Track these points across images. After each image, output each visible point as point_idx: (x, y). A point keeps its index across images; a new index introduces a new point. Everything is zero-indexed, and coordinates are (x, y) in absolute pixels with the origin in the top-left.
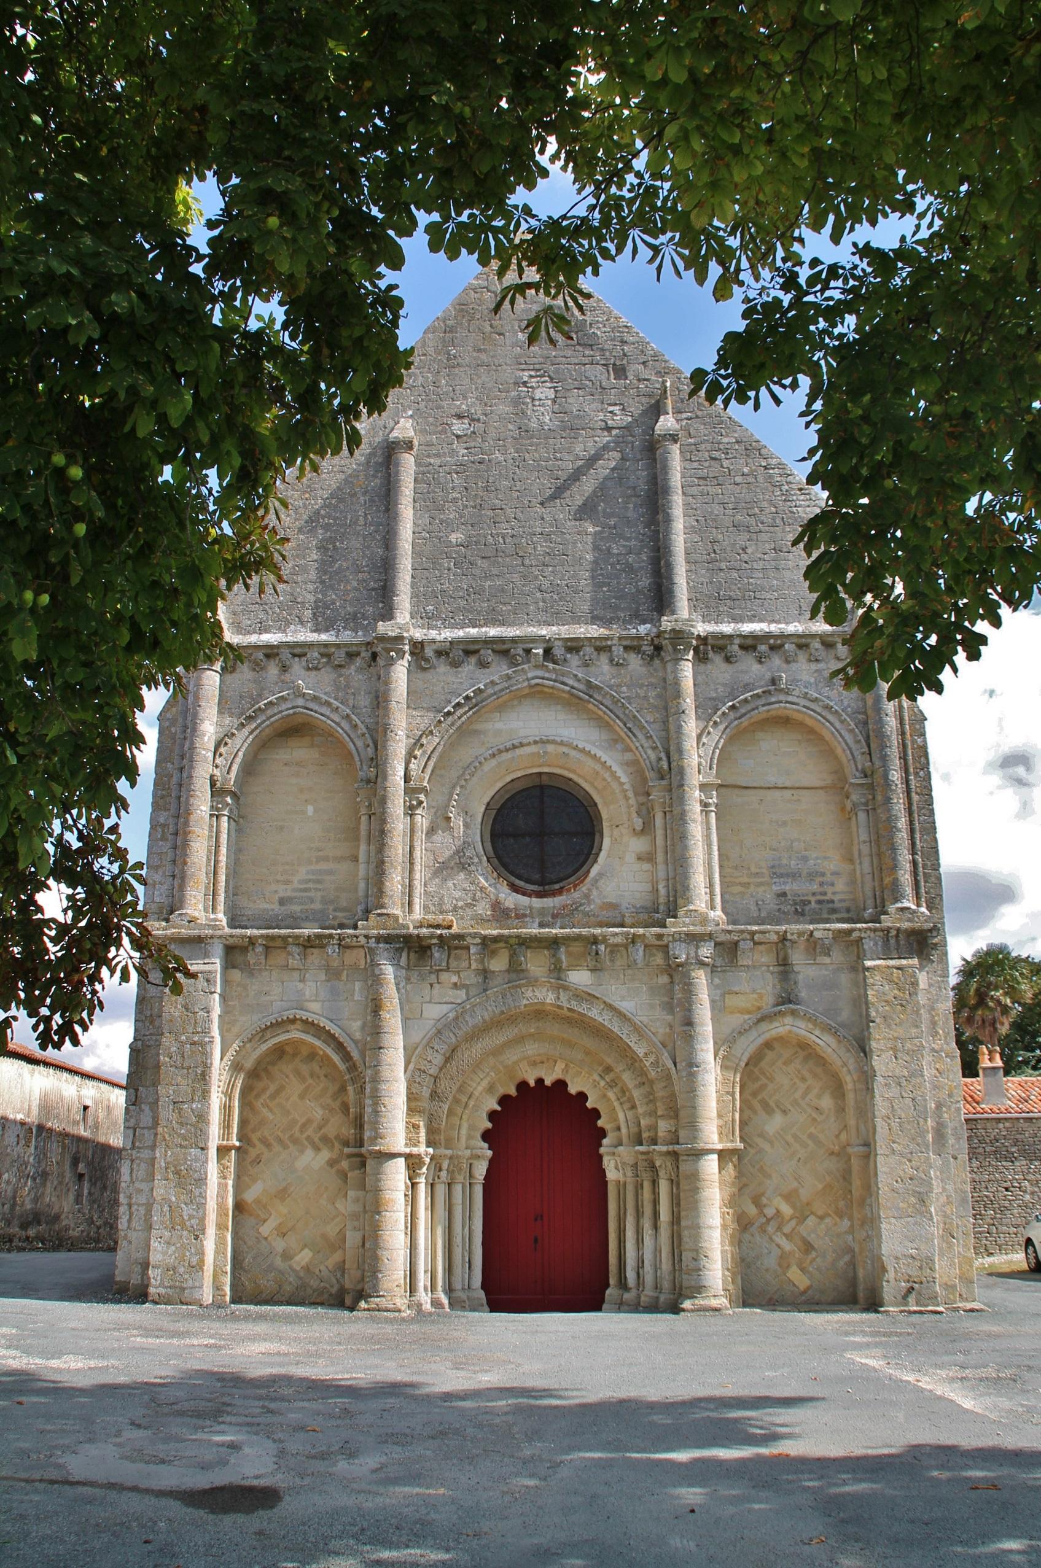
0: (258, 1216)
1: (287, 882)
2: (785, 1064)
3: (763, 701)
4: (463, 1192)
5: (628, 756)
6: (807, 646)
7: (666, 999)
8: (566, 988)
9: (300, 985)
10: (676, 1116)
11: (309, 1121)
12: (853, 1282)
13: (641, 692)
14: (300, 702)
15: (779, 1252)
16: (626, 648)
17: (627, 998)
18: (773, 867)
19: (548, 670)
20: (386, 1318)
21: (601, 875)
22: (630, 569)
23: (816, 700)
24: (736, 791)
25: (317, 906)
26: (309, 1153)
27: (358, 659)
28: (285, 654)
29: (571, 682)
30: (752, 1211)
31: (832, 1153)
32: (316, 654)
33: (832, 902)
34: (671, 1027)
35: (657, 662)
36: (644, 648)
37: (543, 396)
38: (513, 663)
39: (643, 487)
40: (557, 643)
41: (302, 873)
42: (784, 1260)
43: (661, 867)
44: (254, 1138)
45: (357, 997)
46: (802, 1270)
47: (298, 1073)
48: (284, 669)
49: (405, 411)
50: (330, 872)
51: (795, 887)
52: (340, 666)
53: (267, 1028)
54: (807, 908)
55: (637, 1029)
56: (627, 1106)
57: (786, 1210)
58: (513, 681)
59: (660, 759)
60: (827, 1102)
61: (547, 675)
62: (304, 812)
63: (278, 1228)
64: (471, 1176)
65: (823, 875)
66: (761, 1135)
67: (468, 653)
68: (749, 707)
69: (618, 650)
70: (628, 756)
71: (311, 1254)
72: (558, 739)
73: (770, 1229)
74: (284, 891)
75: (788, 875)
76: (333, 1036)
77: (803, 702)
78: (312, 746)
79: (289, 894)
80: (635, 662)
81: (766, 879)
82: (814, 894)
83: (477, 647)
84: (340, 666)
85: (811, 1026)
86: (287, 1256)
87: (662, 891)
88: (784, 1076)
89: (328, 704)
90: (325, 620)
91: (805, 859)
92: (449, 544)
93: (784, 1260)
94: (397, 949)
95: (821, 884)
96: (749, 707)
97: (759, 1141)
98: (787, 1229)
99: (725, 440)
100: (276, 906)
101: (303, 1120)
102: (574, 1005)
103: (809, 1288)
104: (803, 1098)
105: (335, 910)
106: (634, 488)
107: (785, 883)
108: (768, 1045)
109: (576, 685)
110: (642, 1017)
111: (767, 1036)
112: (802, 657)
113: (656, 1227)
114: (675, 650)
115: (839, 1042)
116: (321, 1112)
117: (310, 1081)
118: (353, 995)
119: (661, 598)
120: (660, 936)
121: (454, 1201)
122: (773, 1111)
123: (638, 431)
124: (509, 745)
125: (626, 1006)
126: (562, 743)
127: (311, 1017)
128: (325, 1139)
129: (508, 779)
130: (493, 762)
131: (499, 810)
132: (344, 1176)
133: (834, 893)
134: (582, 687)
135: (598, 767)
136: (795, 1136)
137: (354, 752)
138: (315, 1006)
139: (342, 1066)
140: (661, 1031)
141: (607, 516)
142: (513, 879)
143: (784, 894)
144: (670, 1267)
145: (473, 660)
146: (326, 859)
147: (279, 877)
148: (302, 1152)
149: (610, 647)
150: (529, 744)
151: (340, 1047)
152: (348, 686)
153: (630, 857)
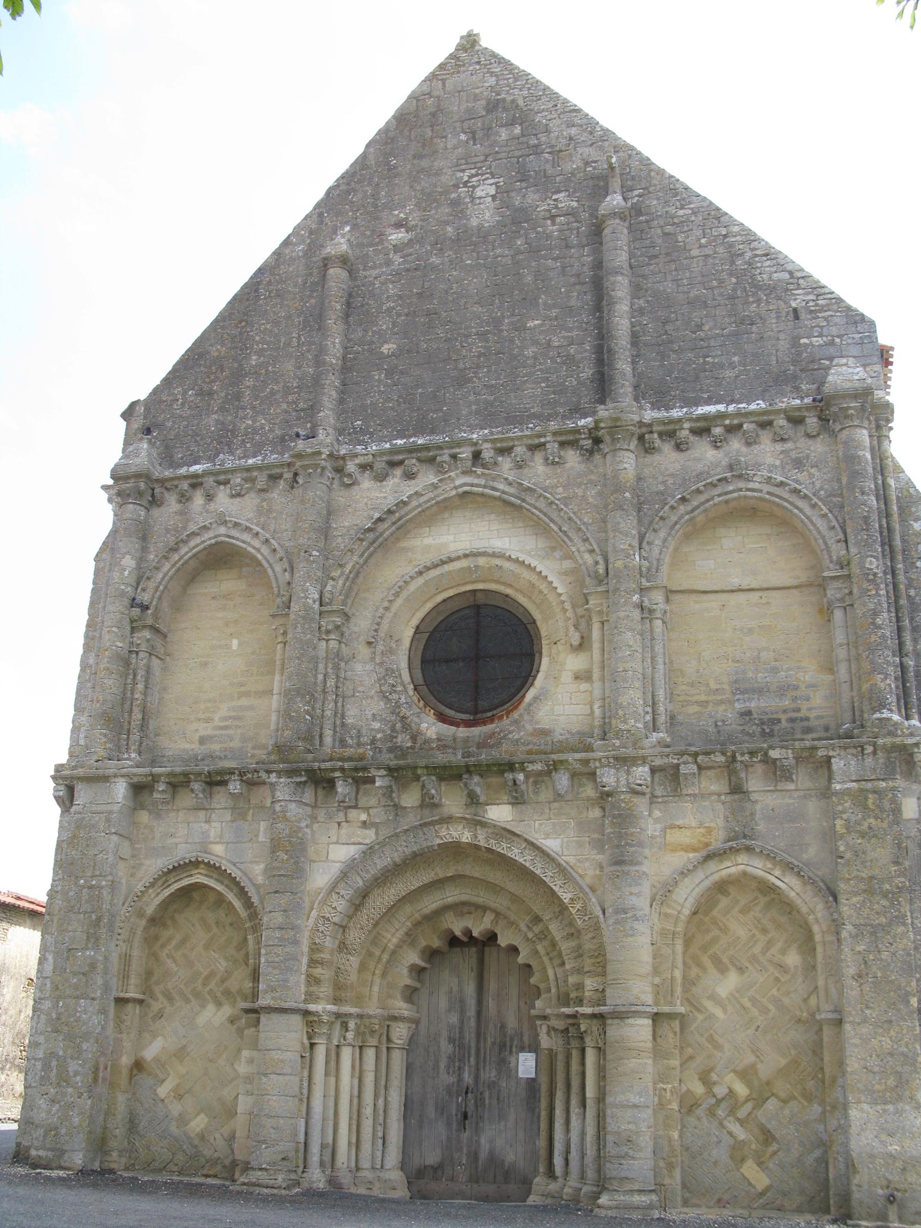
0: (156, 1076)
1: (208, 720)
2: (741, 912)
3: (719, 490)
4: (377, 1058)
5: (567, 564)
6: (770, 423)
7: (596, 836)
8: (483, 824)
9: (205, 826)
10: (604, 974)
11: (212, 974)
12: (825, 1185)
13: (579, 492)
14: (222, 530)
15: (731, 1141)
16: (562, 444)
17: (554, 835)
18: (736, 682)
19: (479, 476)
20: (48, 1178)
21: (536, 699)
22: (570, 361)
23: (782, 484)
24: (694, 597)
25: (236, 744)
26: (211, 1007)
27: (282, 482)
28: (210, 481)
29: (501, 486)
30: (699, 1089)
31: (799, 1021)
32: (239, 480)
33: (807, 719)
34: (601, 868)
35: (597, 457)
36: (582, 442)
37: (482, 194)
38: (440, 469)
39: (588, 273)
40: (487, 445)
41: (224, 710)
42: (738, 1153)
43: (597, 685)
44: (157, 990)
45: (261, 838)
46: (760, 1164)
47: (203, 920)
48: (209, 497)
49: (342, 228)
50: (251, 708)
51: (763, 704)
52: (263, 490)
53: (170, 871)
54: (776, 728)
55: (563, 871)
56: (557, 962)
57: (741, 1090)
58: (440, 490)
59: (597, 563)
60: (793, 959)
61: (476, 481)
62: (228, 646)
63: (176, 1089)
64: (389, 1040)
65: (796, 688)
66: (713, 997)
67: (393, 464)
68: (702, 498)
69: (552, 447)
70: (567, 564)
71: (206, 1120)
72: (490, 551)
73: (720, 1113)
74: (205, 730)
75: (754, 691)
76: (237, 884)
77: (766, 488)
78: (240, 577)
79: (210, 732)
80: (572, 457)
81: (728, 695)
82: (785, 711)
83: (401, 457)
84: (263, 490)
85: (769, 865)
86: (183, 1120)
87: (597, 712)
88: (738, 925)
89: (248, 529)
90: (254, 445)
91: (775, 670)
92: (382, 357)
93: (738, 1153)
94: (298, 784)
95: (795, 699)
96: (702, 498)
97: (709, 1004)
98: (742, 1113)
99: (681, 213)
100: (196, 746)
101: (205, 973)
102: (493, 844)
103: (768, 1189)
104: (764, 953)
105: (253, 748)
106: (578, 275)
107: (750, 700)
108: (721, 887)
109: (507, 489)
110: (568, 858)
111: (716, 877)
112: (765, 437)
113: (583, 1104)
114: (613, 440)
115: (804, 884)
116: (224, 964)
117: (215, 930)
118: (257, 836)
119: (603, 387)
120: (586, 762)
121: (365, 1067)
122: (727, 969)
123: (585, 215)
124: (436, 560)
125: (552, 844)
126: (494, 555)
127: (213, 860)
128: (227, 993)
129: (439, 598)
130: (420, 581)
131: (432, 633)
132: (240, 1031)
133: (810, 709)
134: (512, 490)
135: (534, 578)
136: (753, 1000)
137: (272, 578)
138: (219, 849)
139: (243, 913)
140: (590, 873)
141: (548, 307)
142: (443, 708)
143: (749, 713)
144: (594, 1152)
145: (398, 472)
146: (247, 694)
147: (201, 715)
148: (203, 1006)
149: (544, 444)
150: (458, 558)
151: (242, 893)
152: (270, 511)
153: (566, 676)
